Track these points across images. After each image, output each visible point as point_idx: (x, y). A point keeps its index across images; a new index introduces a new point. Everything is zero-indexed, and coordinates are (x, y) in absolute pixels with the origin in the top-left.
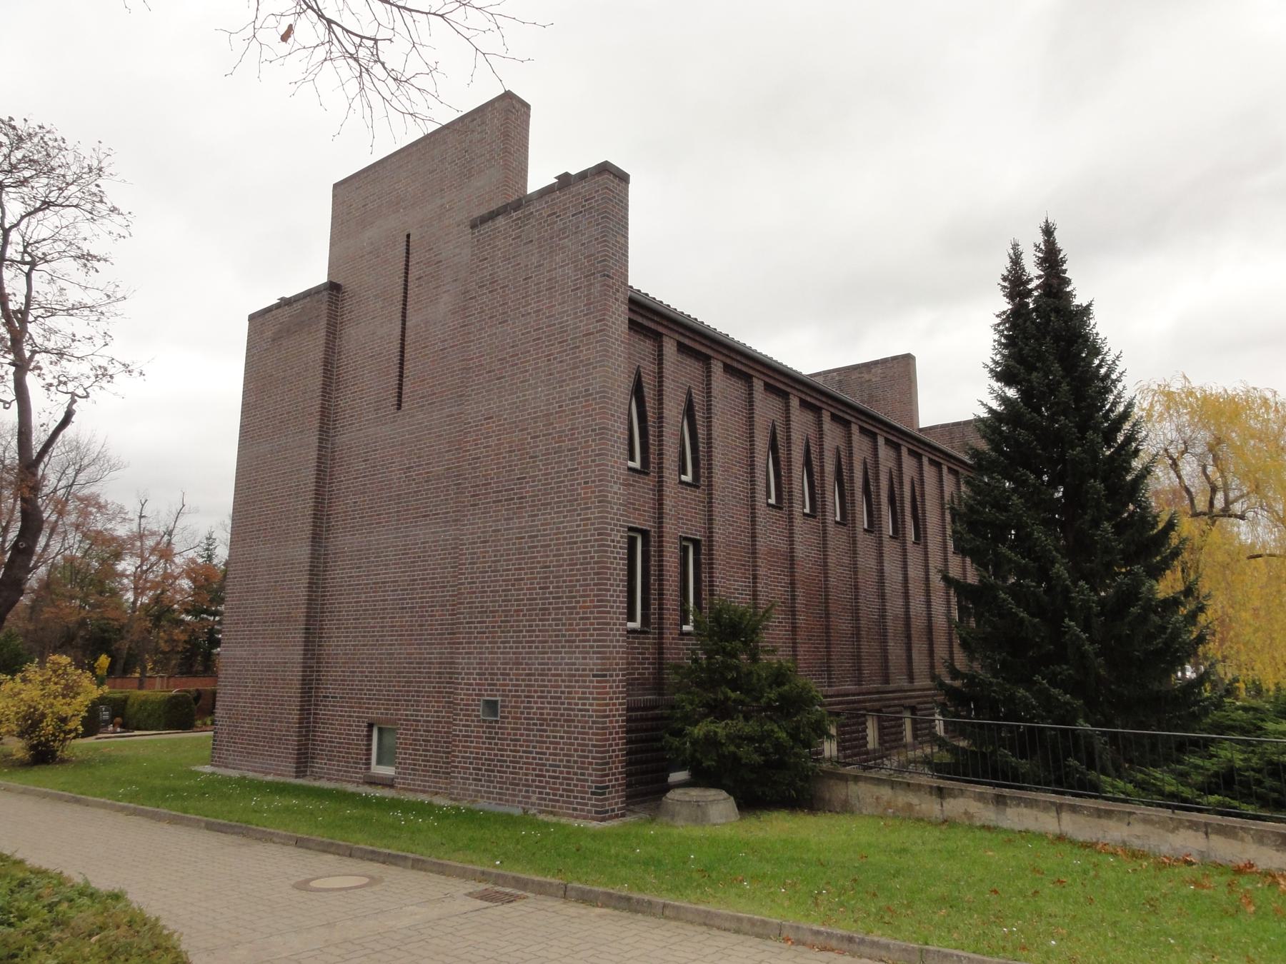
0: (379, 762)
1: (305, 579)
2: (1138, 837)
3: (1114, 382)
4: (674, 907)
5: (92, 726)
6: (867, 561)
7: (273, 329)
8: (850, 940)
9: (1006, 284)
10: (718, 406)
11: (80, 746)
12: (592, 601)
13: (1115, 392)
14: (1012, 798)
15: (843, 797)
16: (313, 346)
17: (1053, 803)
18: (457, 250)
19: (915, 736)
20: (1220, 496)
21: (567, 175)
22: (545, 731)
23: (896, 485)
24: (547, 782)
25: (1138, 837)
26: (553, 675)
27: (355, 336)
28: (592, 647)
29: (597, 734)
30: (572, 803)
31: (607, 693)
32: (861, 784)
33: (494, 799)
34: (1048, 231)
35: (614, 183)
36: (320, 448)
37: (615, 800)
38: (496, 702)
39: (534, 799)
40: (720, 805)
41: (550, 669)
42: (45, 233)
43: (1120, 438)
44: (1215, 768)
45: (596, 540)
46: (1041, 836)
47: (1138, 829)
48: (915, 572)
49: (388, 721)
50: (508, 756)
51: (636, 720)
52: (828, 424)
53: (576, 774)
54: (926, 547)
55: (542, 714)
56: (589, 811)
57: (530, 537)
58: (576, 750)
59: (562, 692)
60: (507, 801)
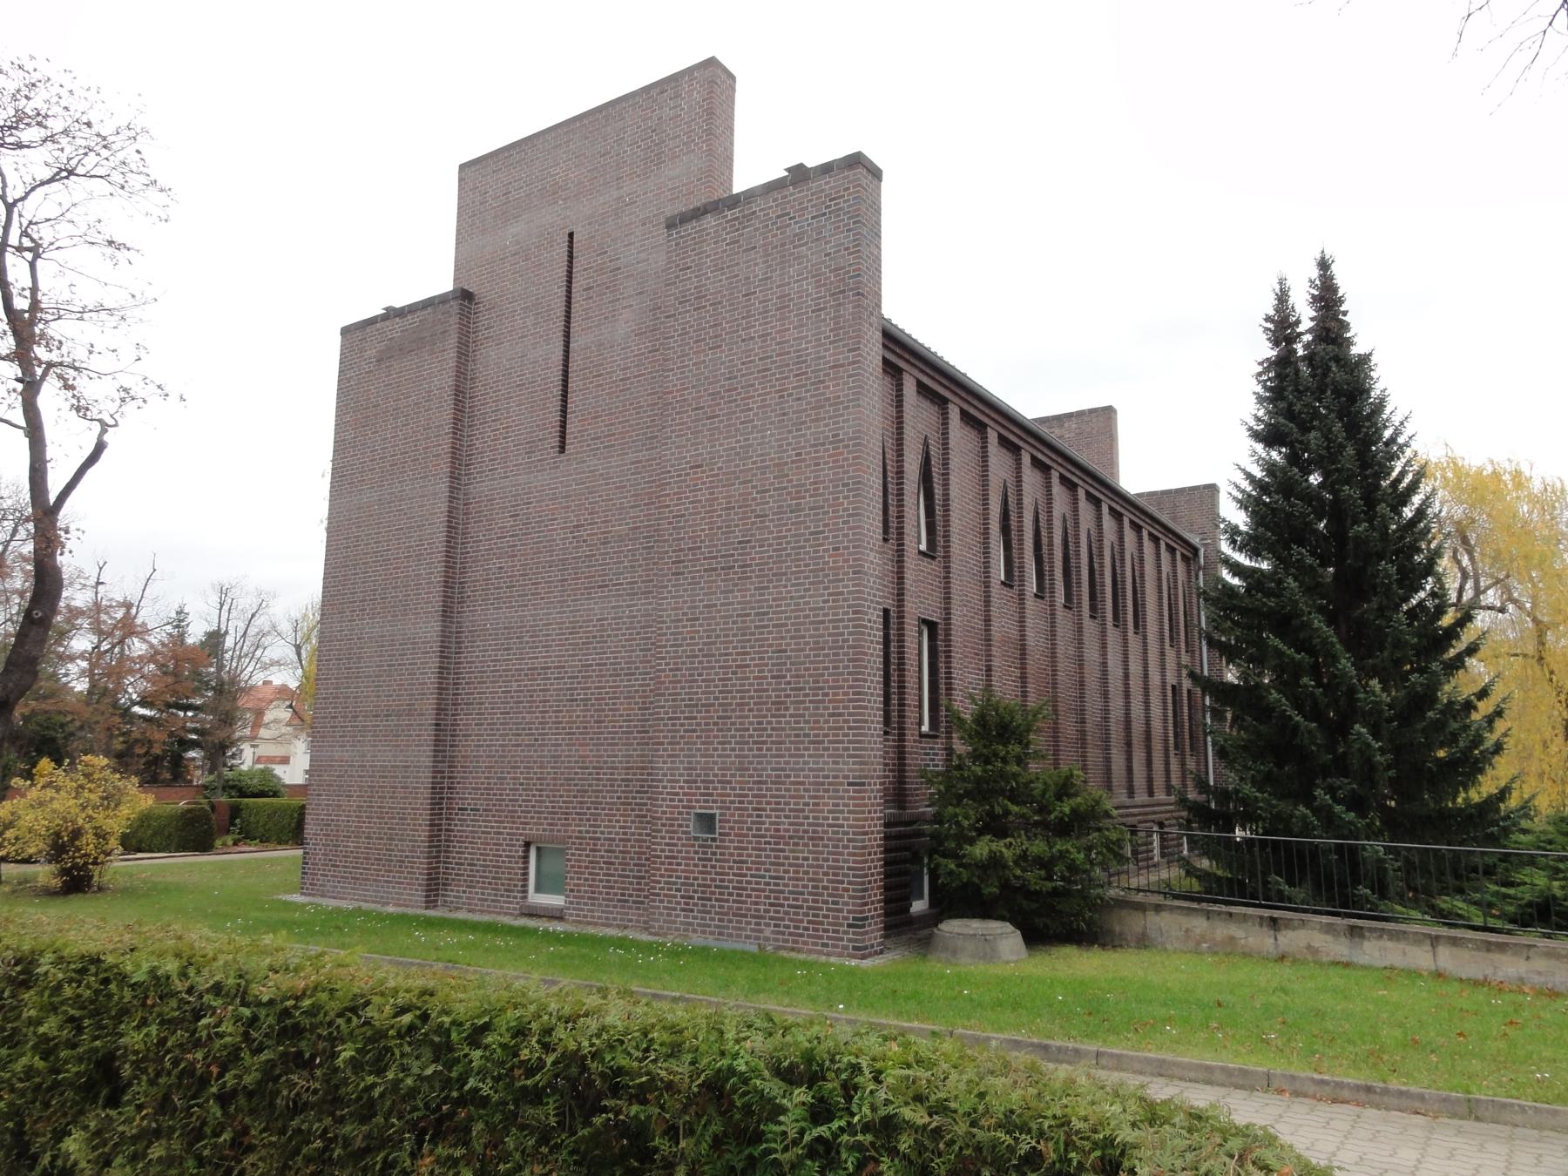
0: (538, 890)
1: (433, 662)
2: (1539, 973)
3: (1401, 448)
4: (1112, 1055)
5: (133, 843)
7: (378, 351)
8: (1369, 1089)
9: (1271, 326)
10: (955, 461)
11: (120, 867)
14: (1371, 930)
15: (1139, 930)
16: (439, 371)
18: (643, 256)
19: (1163, 855)
20: (1469, 585)
21: (801, 166)
22: (783, 851)
24: (787, 913)
25: (1539, 973)
26: (792, 783)
27: (493, 359)
28: (847, 749)
30: (821, 937)
31: (865, 805)
32: (1165, 915)
33: (712, 933)
34: (1324, 265)
35: (866, 179)
36: (452, 499)
38: (712, 816)
39: (768, 932)
40: (1007, 937)
44: (1528, 897)
47: (1540, 964)
48: (1135, 668)
50: (730, 881)
52: (1057, 488)
53: (826, 902)
54: (1145, 638)
55: (778, 830)
57: (757, 614)
58: (826, 874)
60: (730, 935)
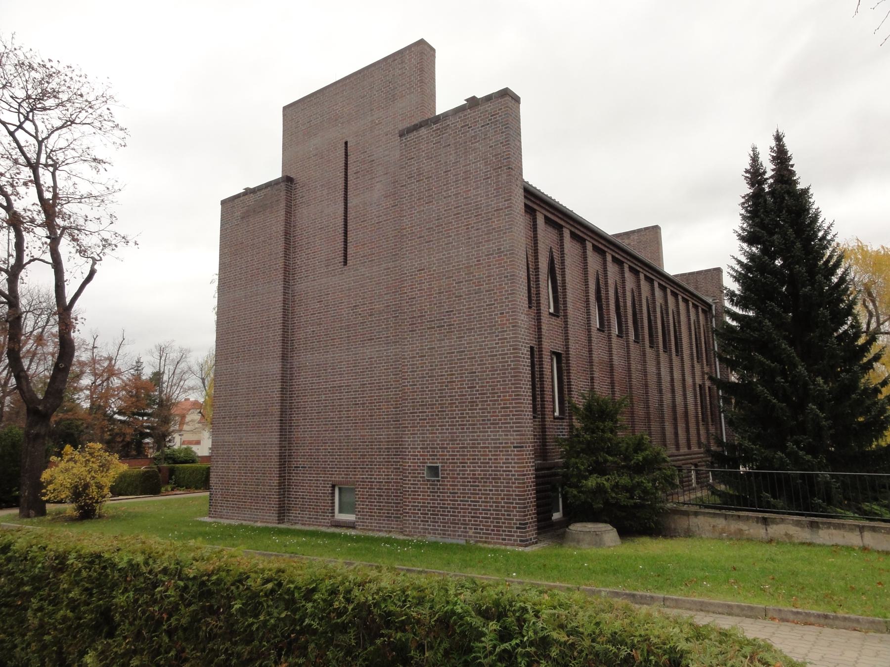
0: (340, 512)
1: (278, 385)
6: (651, 368)
7: (240, 211)
8: (826, 617)
10: (568, 261)
11: (111, 504)
12: (510, 396)
13: (831, 249)
14: (823, 523)
15: (686, 527)
16: (276, 222)
17: (858, 526)
20: (874, 320)
21: (474, 98)
23: (665, 316)
27: (305, 215)
28: (512, 427)
29: (518, 487)
32: (699, 517)
33: (439, 534)
34: (779, 138)
35: (511, 103)
36: (285, 293)
37: (532, 533)
39: (471, 533)
40: (609, 534)
41: (479, 444)
42: (62, 143)
43: (835, 280)
45: (511, 353)
46: (850, 548)
49: (347, 483)
50: (449, 504)
51: (544, 476)
56: (515, 540)
58: (502, 499)
59: (490, 459)
60: (449, 535)
